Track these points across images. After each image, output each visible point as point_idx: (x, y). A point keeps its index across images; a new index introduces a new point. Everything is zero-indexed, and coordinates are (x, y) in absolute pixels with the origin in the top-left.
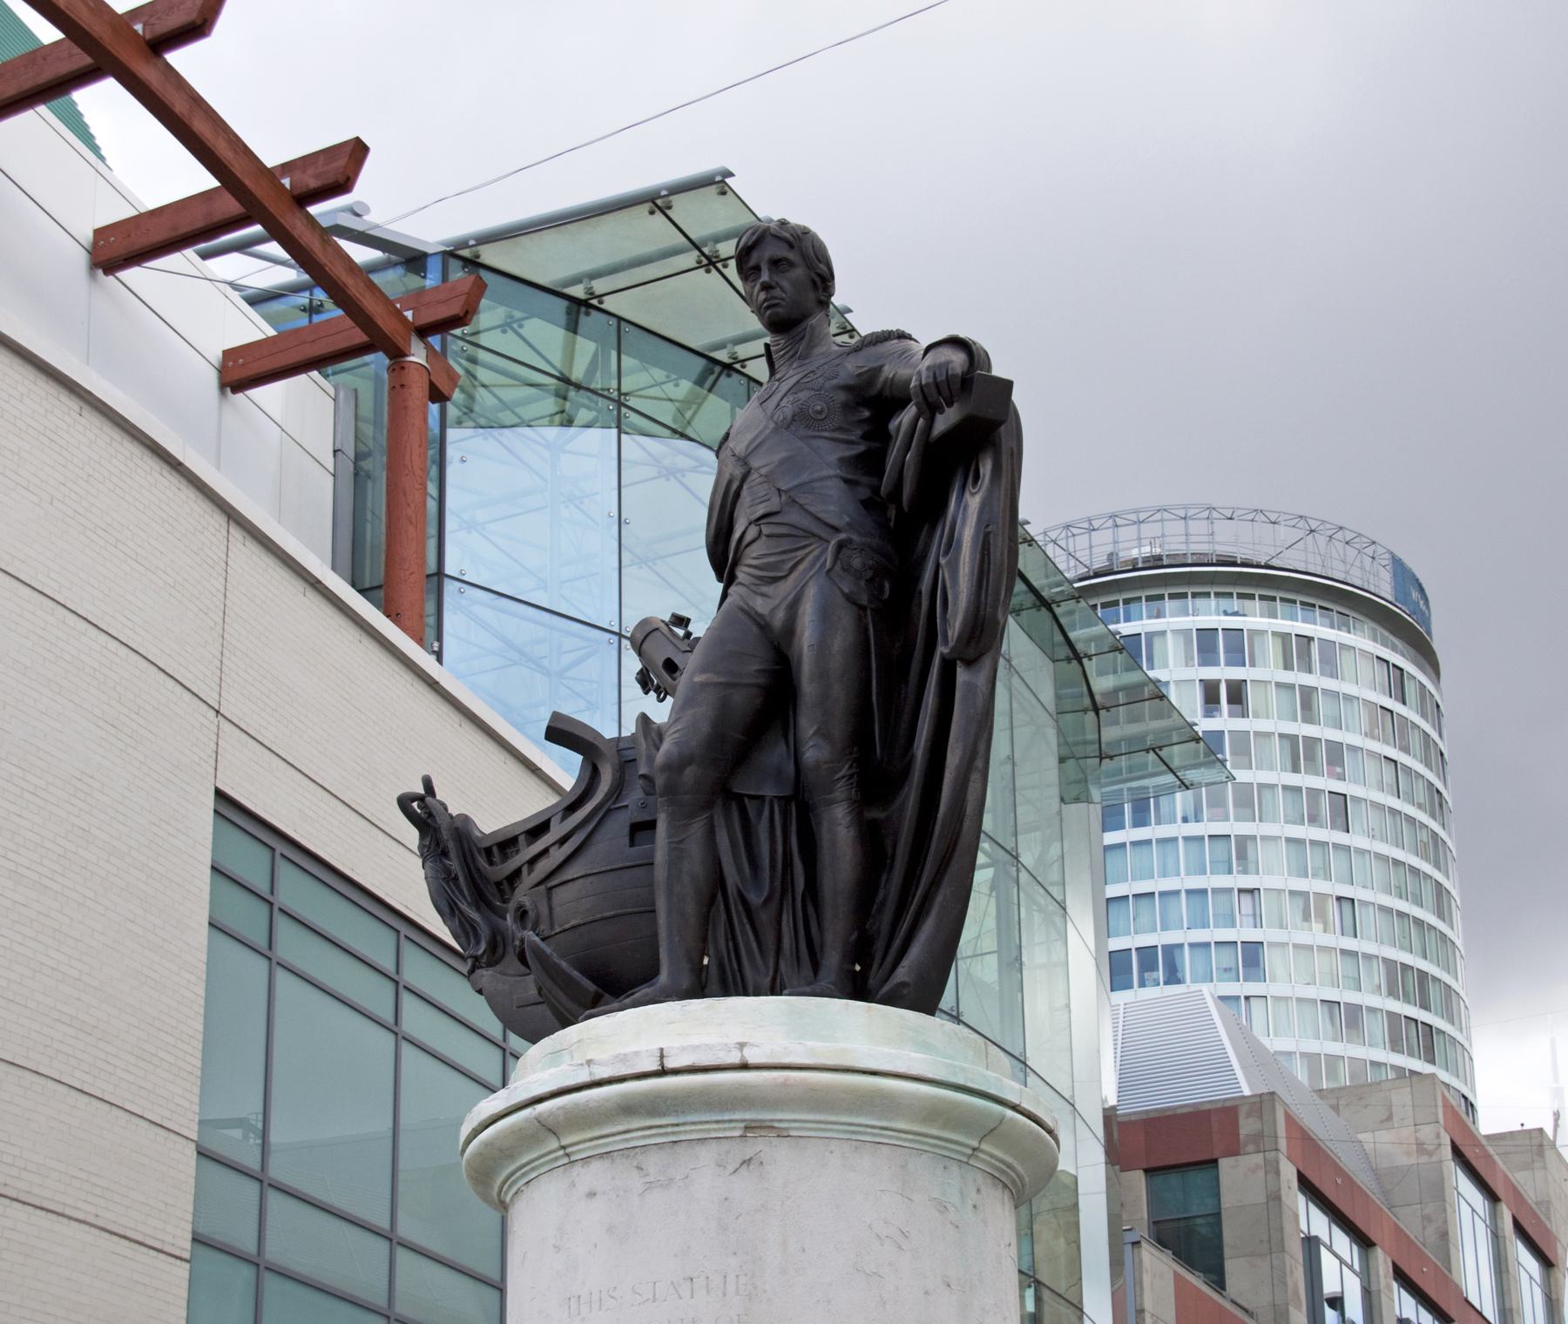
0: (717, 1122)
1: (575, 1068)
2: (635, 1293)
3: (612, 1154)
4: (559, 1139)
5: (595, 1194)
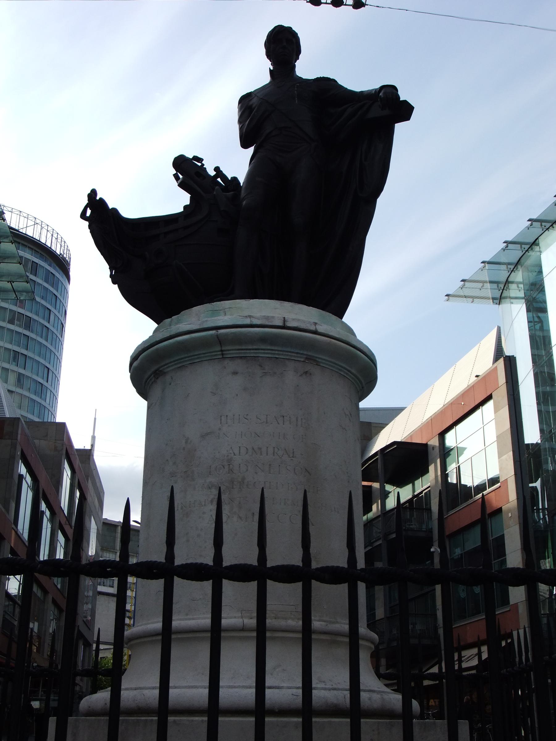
0: (297, 353)
1: (243, 318)
2: (258, 418)
3: (247, 357)
4: (221, 346)
5: (237, 373)
